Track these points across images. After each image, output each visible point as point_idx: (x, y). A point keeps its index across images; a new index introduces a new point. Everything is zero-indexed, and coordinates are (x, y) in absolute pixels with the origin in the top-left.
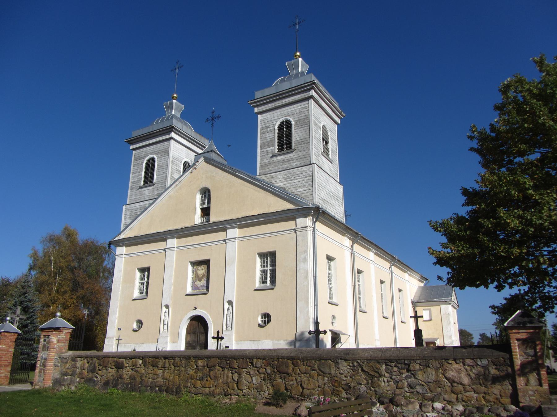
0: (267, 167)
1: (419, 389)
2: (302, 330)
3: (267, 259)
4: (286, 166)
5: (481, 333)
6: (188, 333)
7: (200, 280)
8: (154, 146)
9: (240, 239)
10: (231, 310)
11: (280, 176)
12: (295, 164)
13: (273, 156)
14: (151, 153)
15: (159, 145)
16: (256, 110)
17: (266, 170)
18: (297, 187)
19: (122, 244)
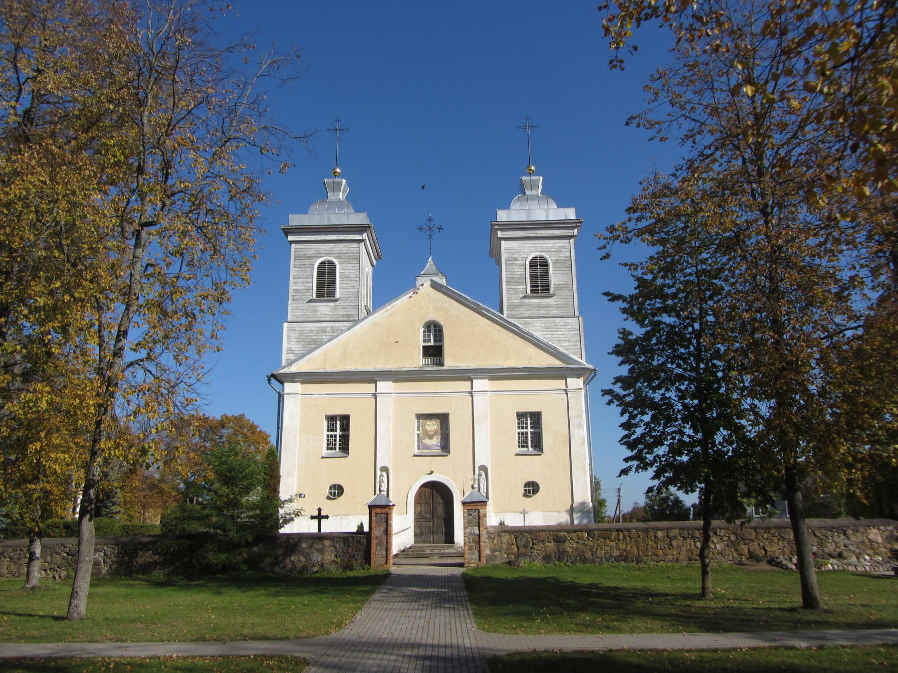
1: (851, 548)
2: (581, 501)
3: (526, 419)
4: (543, 312)
5: (327, 492)
6: (417, 502)
7: (431, 438)
8: (332, 245)
9: (493, 393)
10: (484, 476)
12: (554, 312)
13: (524, 297)
14: (327, 255)
15: (341, 245)
16: (499, 233)
17: (516, 312)
18: (560, 341)
19: (297, 379)
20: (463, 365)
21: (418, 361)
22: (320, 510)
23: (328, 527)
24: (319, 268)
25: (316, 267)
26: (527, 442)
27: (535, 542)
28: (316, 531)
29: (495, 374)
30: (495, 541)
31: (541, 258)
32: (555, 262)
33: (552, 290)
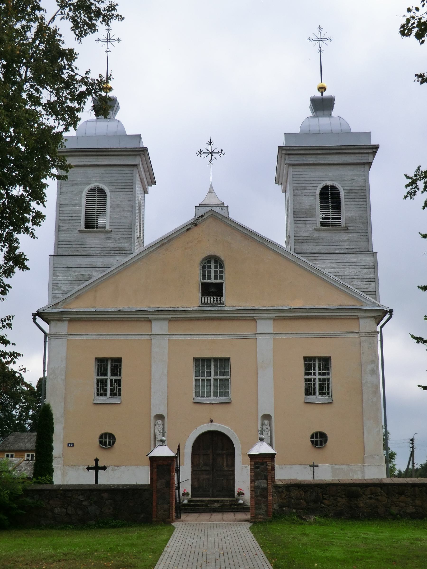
0: (305, 244)
4: (334, 247)
11: (328, 260)
20: (247, 306)
21: (192, 299)
22: (97, 461)
23: (106, 479)
24: (88, 196)
25: (84, 194)
26: (315, 390)
27: (325, 496)
28: (93, 483)
29: (283, 316)
30: (284, 495)
31: (333, 187)
32: (349, 192)
33: (343, 224)
